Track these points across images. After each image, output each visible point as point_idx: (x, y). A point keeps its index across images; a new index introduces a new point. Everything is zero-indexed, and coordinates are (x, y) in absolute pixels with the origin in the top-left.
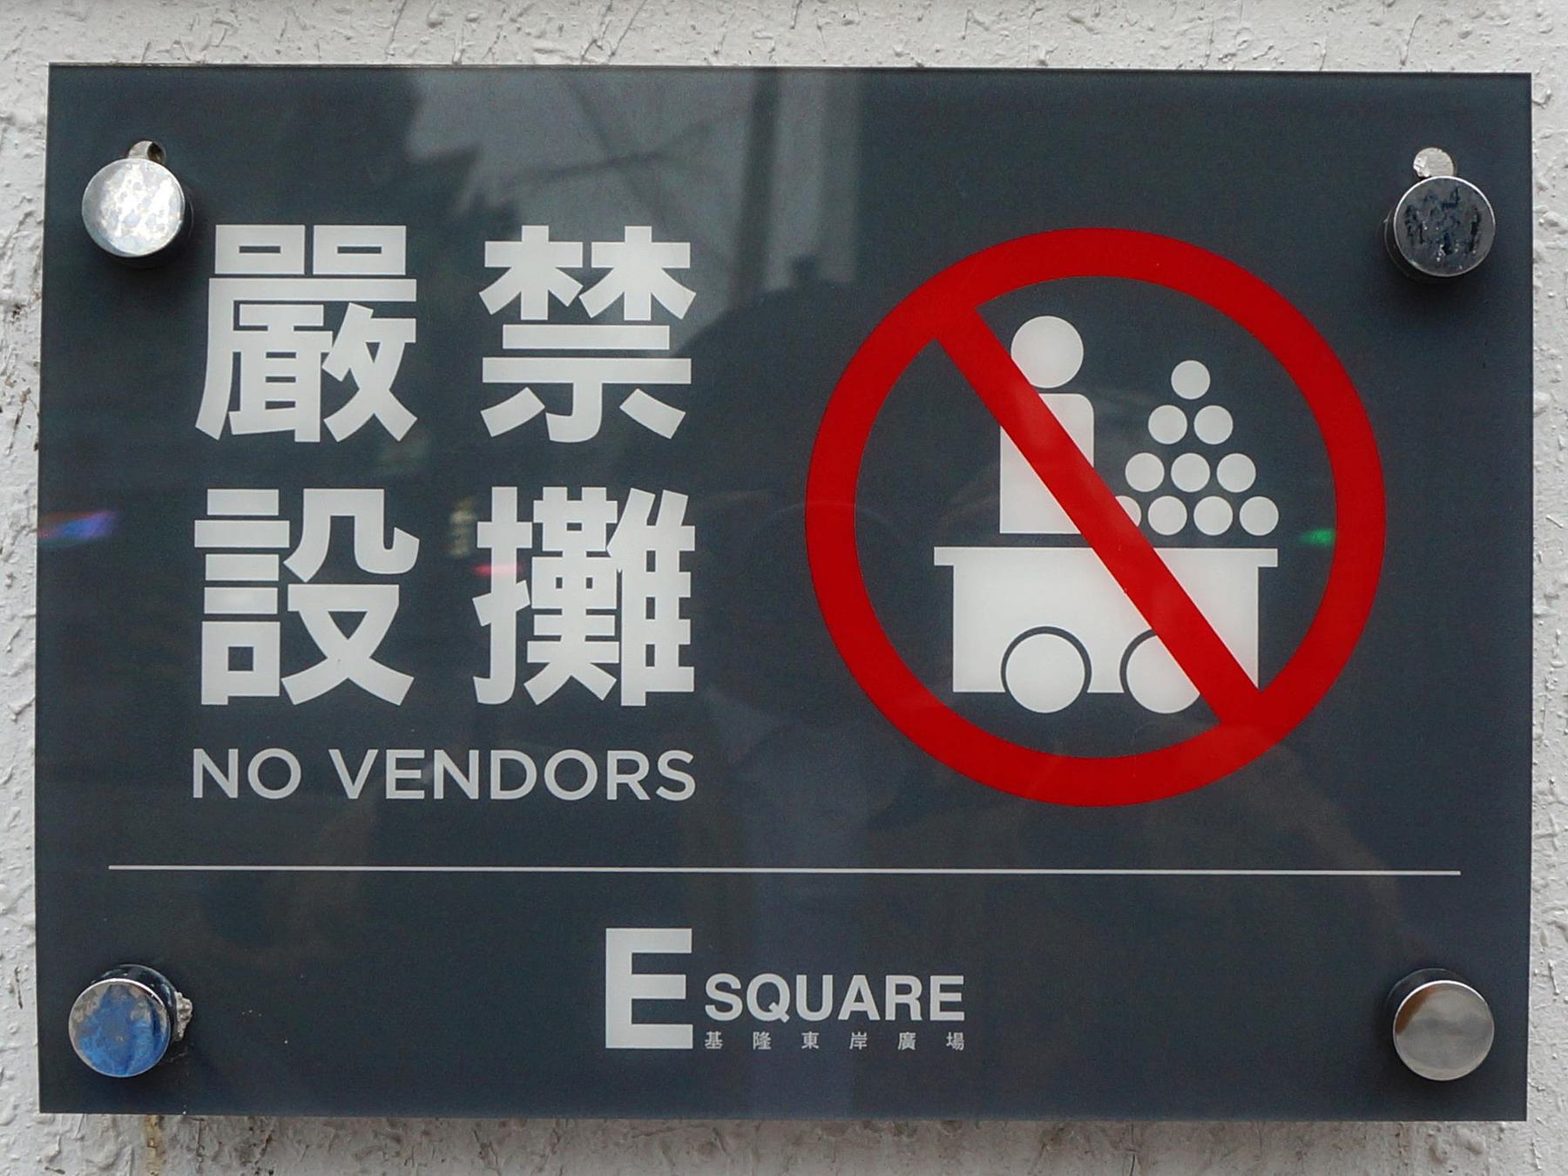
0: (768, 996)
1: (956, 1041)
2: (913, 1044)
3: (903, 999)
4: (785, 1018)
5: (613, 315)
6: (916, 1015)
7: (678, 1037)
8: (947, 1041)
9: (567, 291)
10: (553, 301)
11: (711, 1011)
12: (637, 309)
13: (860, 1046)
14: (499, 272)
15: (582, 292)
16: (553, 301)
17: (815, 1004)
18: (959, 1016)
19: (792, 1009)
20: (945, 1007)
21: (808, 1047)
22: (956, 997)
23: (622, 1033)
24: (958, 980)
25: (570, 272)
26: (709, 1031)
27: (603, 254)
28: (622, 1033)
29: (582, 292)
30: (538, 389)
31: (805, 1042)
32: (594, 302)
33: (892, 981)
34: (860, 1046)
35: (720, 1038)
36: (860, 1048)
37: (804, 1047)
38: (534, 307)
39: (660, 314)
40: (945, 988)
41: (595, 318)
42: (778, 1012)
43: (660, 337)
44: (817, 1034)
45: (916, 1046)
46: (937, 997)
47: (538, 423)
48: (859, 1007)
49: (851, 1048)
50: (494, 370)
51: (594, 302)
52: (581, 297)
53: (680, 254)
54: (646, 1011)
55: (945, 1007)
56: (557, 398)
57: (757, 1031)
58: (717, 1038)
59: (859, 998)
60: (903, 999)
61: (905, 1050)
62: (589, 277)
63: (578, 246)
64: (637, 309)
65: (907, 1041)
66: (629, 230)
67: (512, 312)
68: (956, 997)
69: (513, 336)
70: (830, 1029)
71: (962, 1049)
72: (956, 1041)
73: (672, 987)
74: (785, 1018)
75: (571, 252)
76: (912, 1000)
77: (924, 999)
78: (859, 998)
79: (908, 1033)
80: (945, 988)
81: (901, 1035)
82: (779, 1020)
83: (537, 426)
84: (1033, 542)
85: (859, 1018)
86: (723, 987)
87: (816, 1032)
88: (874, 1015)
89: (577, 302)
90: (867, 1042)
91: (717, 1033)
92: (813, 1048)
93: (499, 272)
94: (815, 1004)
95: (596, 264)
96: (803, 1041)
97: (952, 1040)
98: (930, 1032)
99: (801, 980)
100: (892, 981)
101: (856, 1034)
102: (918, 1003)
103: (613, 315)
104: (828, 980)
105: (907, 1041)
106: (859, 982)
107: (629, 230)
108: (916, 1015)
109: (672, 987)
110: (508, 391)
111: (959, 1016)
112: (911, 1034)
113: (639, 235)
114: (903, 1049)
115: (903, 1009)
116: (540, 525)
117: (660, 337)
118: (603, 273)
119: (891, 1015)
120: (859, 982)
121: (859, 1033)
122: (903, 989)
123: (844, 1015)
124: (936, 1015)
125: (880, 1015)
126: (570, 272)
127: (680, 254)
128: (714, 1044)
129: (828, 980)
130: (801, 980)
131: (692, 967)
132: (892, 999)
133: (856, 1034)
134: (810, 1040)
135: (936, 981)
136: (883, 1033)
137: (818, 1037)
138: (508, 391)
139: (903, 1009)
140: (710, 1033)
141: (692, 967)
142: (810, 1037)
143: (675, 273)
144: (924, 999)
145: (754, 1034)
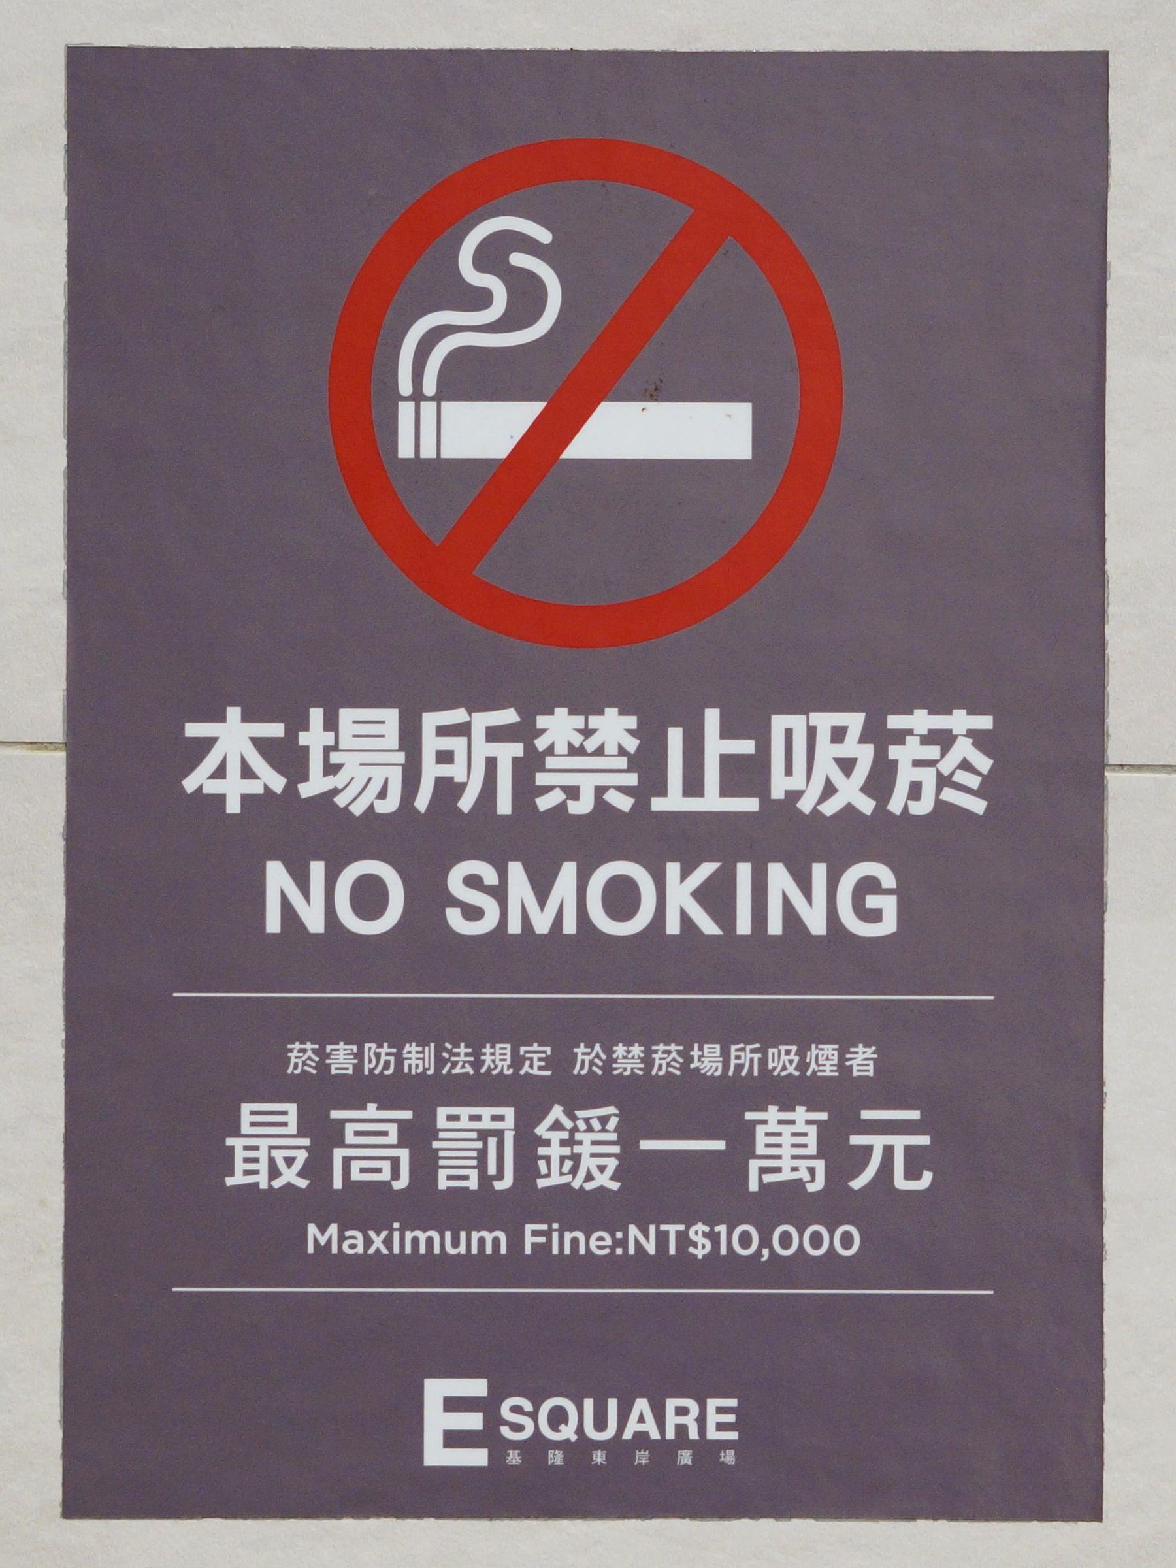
0: (558, 1418)
1: (729, 1457)
2: (690, 1460)
3: (681, 1420)
4: (574, 1438)
5: (600, 751)
6: (693, 1434)
7: (478, 1457)
8: (720, 1457)
9: (577, 740)
10: (570, 746)
11: (505, 1431)
12: (612, 749)
13: (644, 1462)
14: (543, 731)
15: (584, 740)
16: (570, 746)
17: (601, 1424)
18: (733, 1436)
19: (580, 1429)
20: (721, 1427)
21: (597, 1463)
22: (731, 1418)
23: (435, 1455)
24: (732, 1403)
25: (579, 731)
26: (509, 1450)
27: (594, 722)
28: (435, 1455)
29: (584, 740)
30: (564, 789)
31: (594, 1458)
32: (591, 745)
33: (671, 1404)
34: (644, 1462)
35: (519, 1455)
36: (644, 1464)
37: (593, 1463)
38: (562, 748)
39: (622, 751)
40: (720, 1410)
41: (624, 756)
42: (567, 1432)
43: (622, 763)
44: (605, 1452)
45: (692, 1462)
46: (713, 1418)
47: (563, 805)
48: (641, 1428)
49: (636, 1463)
50: (541, 779)
51: (591, 745)
52: (584, 743)
53: (632, 722)
54: (453, 1439)
55: (721, 1427)
56: (573, 792)
57: (552, 1449)
58: (517, 1455)
59: (641, 1419)
60: (681, 1420)
61: (683, 1466)
62: (587, 732)
63: (582, 718)
64: (612, 749)
65: (685, 1458)
66: (607, 710)
67: (550, 751)
68: (731, 1418)
69: (550, 762)
70: (615, 1446)
71: (733, 1463)
72: (729, 1457)
73: (473, 1421)
74: (574, 1438)
75: (578, 722)
76: (690, 1421)
77: (701, 1420)
78: (641, 1419)
79: (686, 1451)
80: (720, 1410)
81: (679, 1452)
82: (568, 1440)
83: (563, 806)
84: (610, 463)
85: (641, 1438)
86: (516, 1409)
87: (680, 1045)
88: (655, 1435)
89: (582, 745)
90: (650, 1459)
91: (517, 1452)
92: (601, 1464)
93: (543, 731)
94: (601, 1424)
95: (591, 727)
96: (592, 1459)
97: (724, 1457)
98: (706, 1449)
99: (589, 1404)
100: (671, 1404)
101: (640, 1451)
102: (696, 1424)
103: (600, 751)
104: (613, 1404)
105: (685, 1458)
106: (642, 1405)
107: (607, 710)
108: (693, 1434)
109: (473, 1421)
110: (548, 789)
111: (733, 1436)
112: (689, 1451)
113: (611, 712)
114: (682, 1464)
115: (681, 1430)
116: (815, 728)
117: (622, 763)
118: (595, 731)
119: (670, 1434)
120: (642, 1405)
121: (642, 1450)
122: (682, 1411)
123: (628, 1435)
124: (712, 1434)
125: (661, 1436)
126: (579, 731)
127: (632, 722)
128: (514, 1461)
129: (613, 1404)
130: (589, 1404)
131: (488, 1406)
132: (672, 1420)
133: (640, 1451)
134: (599, 1457)
135: (712, 1404)
136: (664, 1450)
137: (606, 1454)
138: (548, 789)
139: (681, 1430)
140: (511, 1452)
141: (488, 1406)
142: (599, 1454)
143: (629, 731)
144: (701, 1420)
145: (550, 1452)
